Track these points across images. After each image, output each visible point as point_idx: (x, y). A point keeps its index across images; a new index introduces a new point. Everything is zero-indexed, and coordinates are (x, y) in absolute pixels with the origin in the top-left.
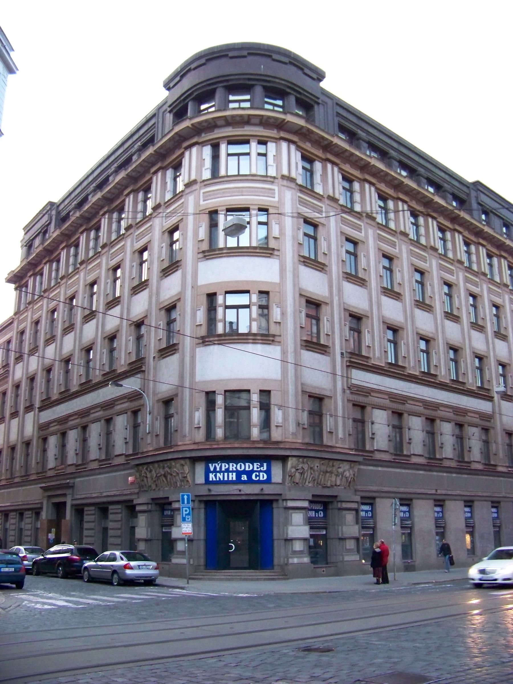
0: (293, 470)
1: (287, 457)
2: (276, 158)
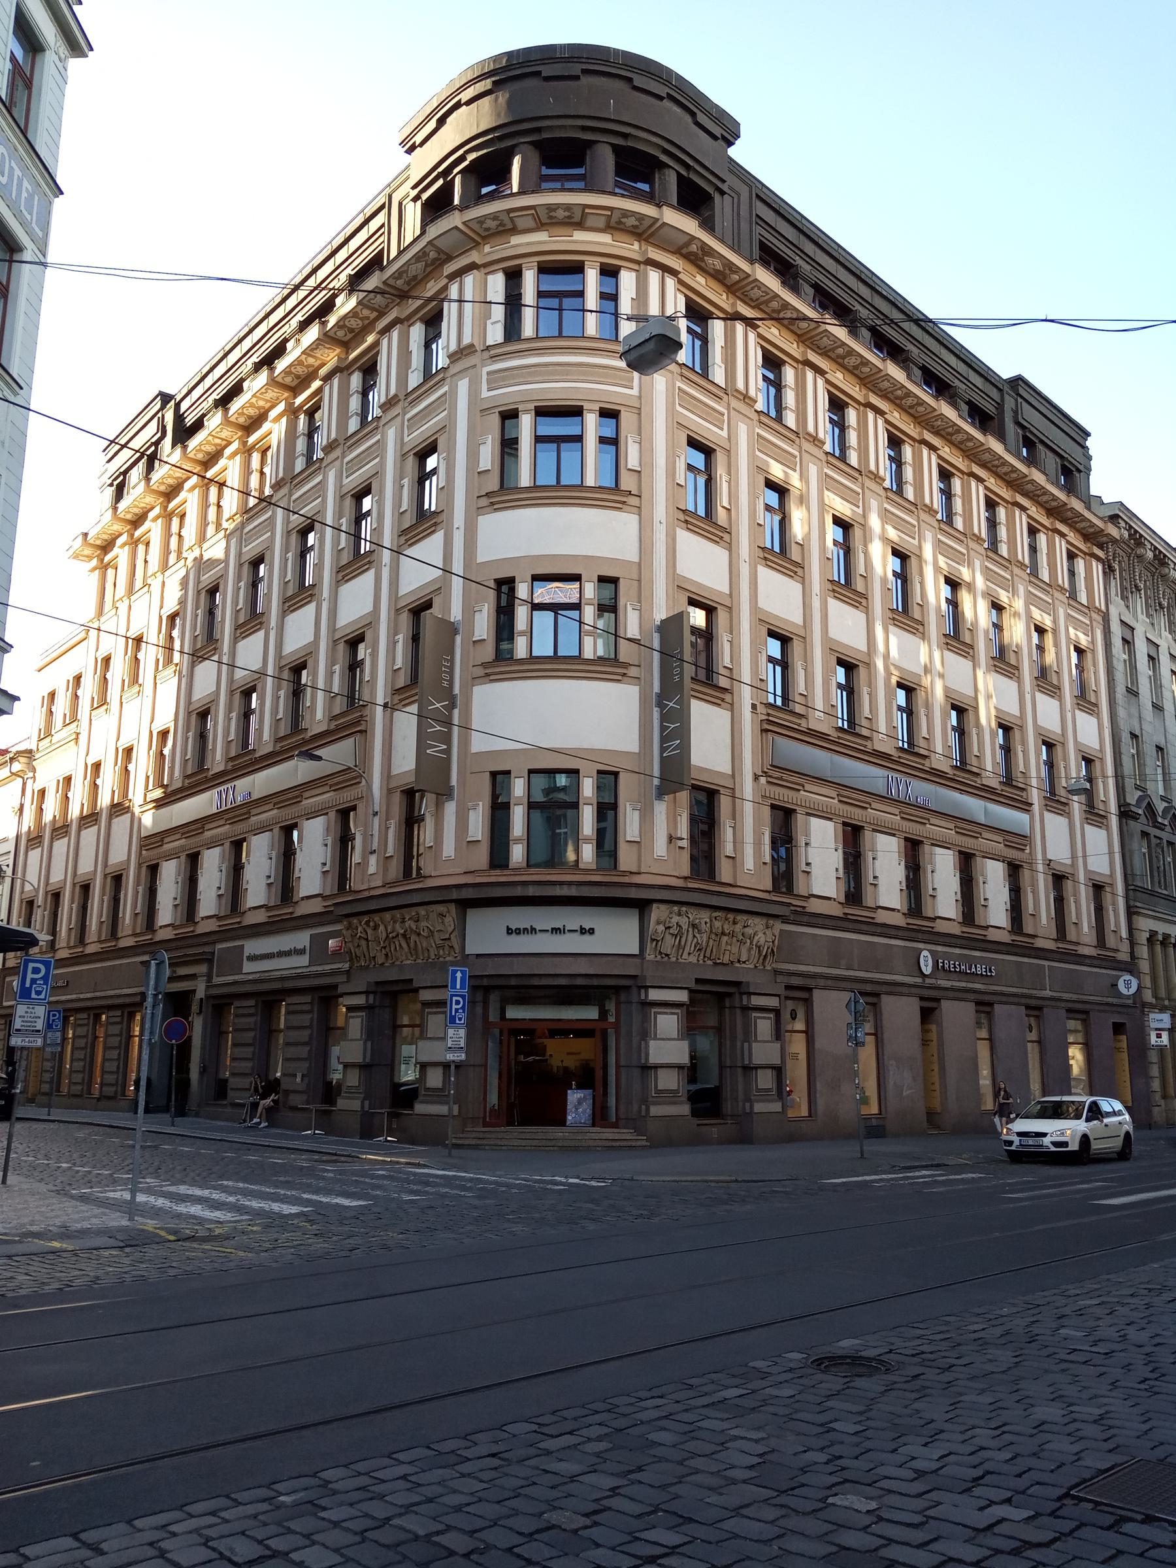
0: (661, 928)
1: (649, 902)
2: (635, 303)
